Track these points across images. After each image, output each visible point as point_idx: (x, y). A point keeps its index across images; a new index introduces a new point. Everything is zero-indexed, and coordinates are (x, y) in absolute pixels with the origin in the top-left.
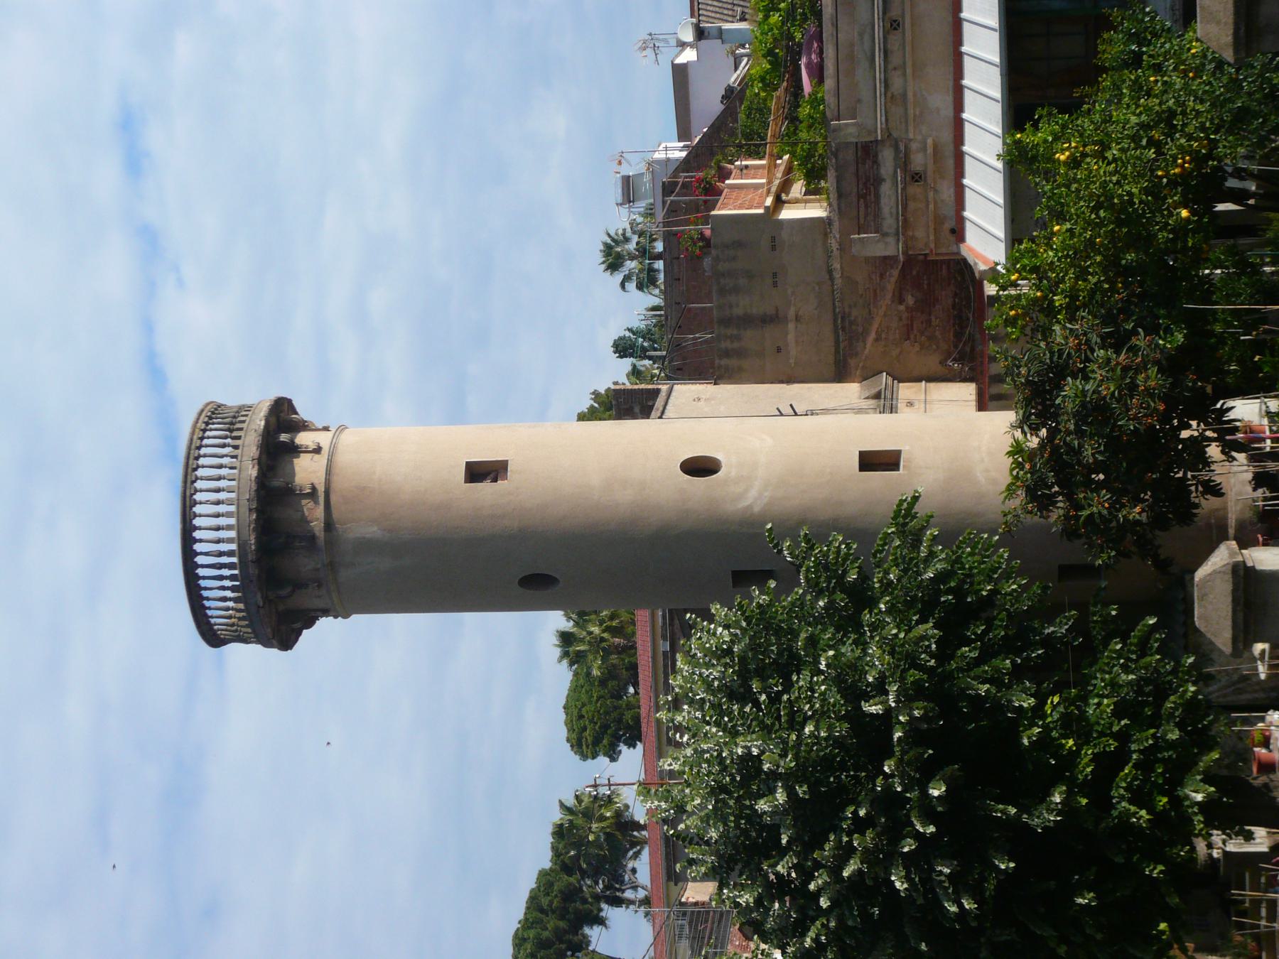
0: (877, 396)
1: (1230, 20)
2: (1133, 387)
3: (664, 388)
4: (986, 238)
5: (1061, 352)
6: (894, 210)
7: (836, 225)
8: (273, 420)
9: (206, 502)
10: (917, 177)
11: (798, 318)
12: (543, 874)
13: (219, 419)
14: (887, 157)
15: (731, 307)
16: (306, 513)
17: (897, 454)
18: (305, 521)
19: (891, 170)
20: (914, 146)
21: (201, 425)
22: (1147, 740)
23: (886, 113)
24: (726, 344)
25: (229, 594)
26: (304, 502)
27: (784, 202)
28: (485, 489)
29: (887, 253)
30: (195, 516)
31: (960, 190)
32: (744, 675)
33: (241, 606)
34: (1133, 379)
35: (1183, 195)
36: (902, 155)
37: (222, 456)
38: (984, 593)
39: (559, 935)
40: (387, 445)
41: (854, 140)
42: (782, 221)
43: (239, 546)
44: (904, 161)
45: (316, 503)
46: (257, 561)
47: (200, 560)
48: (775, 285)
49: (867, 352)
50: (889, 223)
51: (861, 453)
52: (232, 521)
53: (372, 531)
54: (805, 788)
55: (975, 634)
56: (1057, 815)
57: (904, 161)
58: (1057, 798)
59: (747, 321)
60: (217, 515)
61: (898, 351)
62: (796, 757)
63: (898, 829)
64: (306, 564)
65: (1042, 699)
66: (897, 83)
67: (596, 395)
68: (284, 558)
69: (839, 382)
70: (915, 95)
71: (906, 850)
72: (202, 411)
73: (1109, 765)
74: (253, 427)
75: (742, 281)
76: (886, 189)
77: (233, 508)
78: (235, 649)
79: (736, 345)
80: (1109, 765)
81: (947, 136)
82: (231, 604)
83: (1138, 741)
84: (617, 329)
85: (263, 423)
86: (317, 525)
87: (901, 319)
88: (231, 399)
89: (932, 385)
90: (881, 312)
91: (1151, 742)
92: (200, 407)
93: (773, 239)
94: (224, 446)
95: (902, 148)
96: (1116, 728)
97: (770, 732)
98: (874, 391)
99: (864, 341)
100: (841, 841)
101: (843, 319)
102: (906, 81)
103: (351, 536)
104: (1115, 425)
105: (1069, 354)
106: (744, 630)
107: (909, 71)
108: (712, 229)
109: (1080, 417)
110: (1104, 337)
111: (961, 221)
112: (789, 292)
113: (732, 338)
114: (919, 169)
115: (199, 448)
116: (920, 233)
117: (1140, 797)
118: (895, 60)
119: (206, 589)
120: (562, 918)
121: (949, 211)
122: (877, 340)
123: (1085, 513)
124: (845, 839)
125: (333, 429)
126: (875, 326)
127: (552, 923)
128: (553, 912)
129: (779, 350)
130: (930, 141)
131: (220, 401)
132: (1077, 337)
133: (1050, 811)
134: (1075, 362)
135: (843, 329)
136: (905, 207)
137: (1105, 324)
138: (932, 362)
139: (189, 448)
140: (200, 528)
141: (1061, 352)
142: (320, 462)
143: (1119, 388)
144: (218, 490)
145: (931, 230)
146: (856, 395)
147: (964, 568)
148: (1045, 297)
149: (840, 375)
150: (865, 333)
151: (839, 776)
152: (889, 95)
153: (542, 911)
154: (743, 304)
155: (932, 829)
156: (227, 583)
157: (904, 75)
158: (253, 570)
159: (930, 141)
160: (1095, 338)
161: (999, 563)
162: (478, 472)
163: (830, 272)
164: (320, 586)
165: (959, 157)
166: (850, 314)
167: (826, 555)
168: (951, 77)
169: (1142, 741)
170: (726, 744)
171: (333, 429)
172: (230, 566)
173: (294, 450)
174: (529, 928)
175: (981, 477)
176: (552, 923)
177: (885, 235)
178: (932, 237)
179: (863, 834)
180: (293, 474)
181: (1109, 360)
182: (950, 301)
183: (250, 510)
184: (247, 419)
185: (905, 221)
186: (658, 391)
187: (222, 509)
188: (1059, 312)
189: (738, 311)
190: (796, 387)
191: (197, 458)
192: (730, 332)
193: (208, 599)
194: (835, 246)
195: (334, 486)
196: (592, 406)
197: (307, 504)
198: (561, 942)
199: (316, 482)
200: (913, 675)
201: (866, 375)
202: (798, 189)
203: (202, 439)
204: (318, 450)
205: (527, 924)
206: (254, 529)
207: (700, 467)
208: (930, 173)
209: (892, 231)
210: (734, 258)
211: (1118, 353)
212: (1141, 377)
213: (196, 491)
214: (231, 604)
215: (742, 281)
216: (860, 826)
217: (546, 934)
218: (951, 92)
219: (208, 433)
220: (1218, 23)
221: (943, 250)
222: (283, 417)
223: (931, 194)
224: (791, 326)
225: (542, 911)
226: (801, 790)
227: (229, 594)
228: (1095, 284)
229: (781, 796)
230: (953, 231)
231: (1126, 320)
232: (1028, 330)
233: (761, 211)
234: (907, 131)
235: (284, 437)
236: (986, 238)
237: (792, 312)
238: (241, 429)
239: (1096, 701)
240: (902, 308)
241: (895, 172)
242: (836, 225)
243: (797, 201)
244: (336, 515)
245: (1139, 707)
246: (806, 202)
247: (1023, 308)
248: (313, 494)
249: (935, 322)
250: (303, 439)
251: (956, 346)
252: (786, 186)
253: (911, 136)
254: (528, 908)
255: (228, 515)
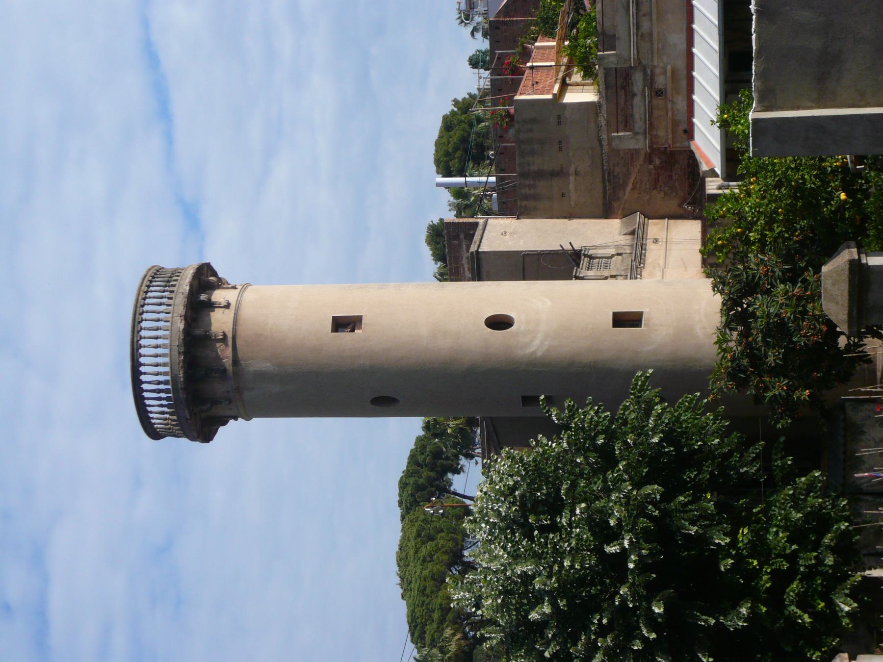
0: (632, 233)
1: (846, 304)
2: (804, 312)
3: (481, 221)
4: (708, 144)
5: (754, 276)
6: (643, 116)
7: (604, 107)
8: (196, 282)
9: (149, 346)
10: (660, 93)
11: (576, 173)
12: (419, 440)
13: (158, 278)
14: (638, 79)
15: (529, 165)
16: (220, 353)
17: (640, 314)
18: (218, 358)
19: (640, 88)
20: (657, 71)
21: (146, 283)
22: (811, 560)
23: (637, 48)
24: (526, 191)
25: (165, 409)
26: (218, 345)
27: (568, 85)
28: (345, 337)
29: (637, 147)
30: (141, 356)
31: (691, 104)
32: (524, 510)
33: (175, 418)
34: (804, 306)
35: (843, 180)
36: (649, 77)
37: (159, 313)
38: (696, 447)
39: (430, 482)
40: (277, 302)
41: (614, 66)
42: (565, 105)
43: (172, 377)
44: (650, 81)
45: (227, 345)
46: (185, 389)
47: (145, 386)
48: (560, 149)
49: (626, 197)
50: (639, 125)
51: (614, 314)
52: (167, 360)
53: (267, 366)
54: (564, 602)
55: (690, 477)
56: (744, 622)
57: (650, 81)
58: (744, 611)
59: (540, 175)
60: (157, 356)
61: (648, 196)
62: (558, 581)
63: (631, 633)
64: (220, 388)
65: (733, 534)
66: (645, 25)
67: (456, 102)
68: (203, 381)
69: (606, 218)
70: (658, 33)
71: (636, 648)
72: (145, 276)
73: (782, 579)
74: (181, 290)
75: (536, 146)
76: (637, 100)
77: (167, 342)
78: (168, 441)
79: (532, 191)
80: (782, 579)
81: (682, 64)
82: (167, 416)
83: (806, 559)
84: (471, 52)
85: (188, 288)
86: (227, 362)
87: (650, 174)
88: (169, 263)
89: (672, 222)
90: (636, 170)
91: (813, 562)
92: (144, 273)
93: (559, 117)
94: (160, 304)
95: (649, 72)
96: (788, 551)
97: (540, 559)
98: (630, 229)
99: (624, 191)
100: (590, 638)
101: (609, 173)
102: (652, 24)
103: (251, 369)
104: (790, 340)
105: (760, 277)
106: (523, 478)
107: (654, 17)
108: (515, 110)
109: (767, 332)
110: (784, 272)
111: (691, 125)
112: (571, 154)
113: (530, 187)
114: (661, 87)
115: (143, 306)
116: (661, 133)
117: (804, 602)
118: (644, 8)
119: (150, 406)
120: (432, 470)
121: (683, 117)
122: (633, 189)
123: (770, 394)
124: (593, 637)
125: (239, 287)
126: (632, 179)
127: (426, 473)
128: (426, 466)
129: (563, 195)
130: (669, 68)
131: (162, 266)
132: (766, 266)
133: (740, 619)
134: (764, 284)
135: (609, 181)
136: (651, 114)
137: (785, 262)
138: (672, 205)
139: (136, 307)
140: (144, 365)
141: (754, 276)
142: (229, 314)
143: (794, 313)
144: (157, 338)
145: (670, 131)
146: (617, 231)
147: (681, 427)
148: (743, 233)
149: (607, 213)
150: (625, 184)
151: (589, 591)
152: (640, 33)
153: (418, 464)
154: (538, 163)
155: (653, 636)
156: (164, 402)
157: (651, 19)
158: (182, 395)
159: (669, 68)
160: (778, 273)
161: (707, 423)
162: (342, 324)
163: (600, 141)
164: (230, 402)
165: (690, 80)
166: (613, 171)
167: (583, 421)
168: (685, 22)
169: (807, 560)
170: (510, 564)
171: (239, 287)
172: (166, 391)
173: (211, 306)
174: (410, 477)
175: (700, 333)
176: (426, 473)
177: (636, 134)
178: (670, 136)
179: (605, 637)
180: (210, 324)
181: (787, 292)
182: (686, 162)
183: (179, 353)
184: (179, 278)
185: (651, 124)
186: (477, 224)
187: (159, 351)
188: (754, 243)
189: (534, 168)
190: (576, 222)
191: (141, 314)
192: (527, 182)
193: (151, 412)
194: (603, 122)
195: (239, 333)
196: (453, 110)
197: (220, 346)
198: (432, 486)
199: (226, 330)
200: (643, 522)
201: (626, 214)
202: (577, 77)
203: (144, 299)
204: (228, 306)
205: (408, 474)
206: (182, 367)
207: (499, 323)
208: (669, 90)
209: (641, 131)
210: (531, 130)
211: (794, 284)
212: (810, 306)
213: (141, 338)
214: (167, 416)
215: (536, 146)
216: (603, 631)
217: (421, 481)
218: (685, 32)
219: (151, 288)
220: (837, 303)
221: (678, 145)
222: (205, 279)
223: (670, 105)
224: (572, 178)
225: (418, 464)
226: (562, 603)
227: (165, 409)
228: (778, 233)
229: (547, 609)
230: (685, 131)
231: (801, 260)
232: (731, 256)
233: (550, 97)
234: (652, 60)
235: (203, 297)
236: (708, 144)
237: (572, 169)
238: (176, 280)
239: (775, 529)
240: (651, 166)
241: (644, 90)
242: (604, 107)
243: (577, 84)
244: (240, 354)
245: (807, 534)
246: (584, 85)
247: (727, 240)
248: (224, 339)
249: (675, 177)
250: (219, 296)
251: (690, 194)
252: (568, 75)
253: (655, 63)
254: (409, 463)
255: (164, 355)
